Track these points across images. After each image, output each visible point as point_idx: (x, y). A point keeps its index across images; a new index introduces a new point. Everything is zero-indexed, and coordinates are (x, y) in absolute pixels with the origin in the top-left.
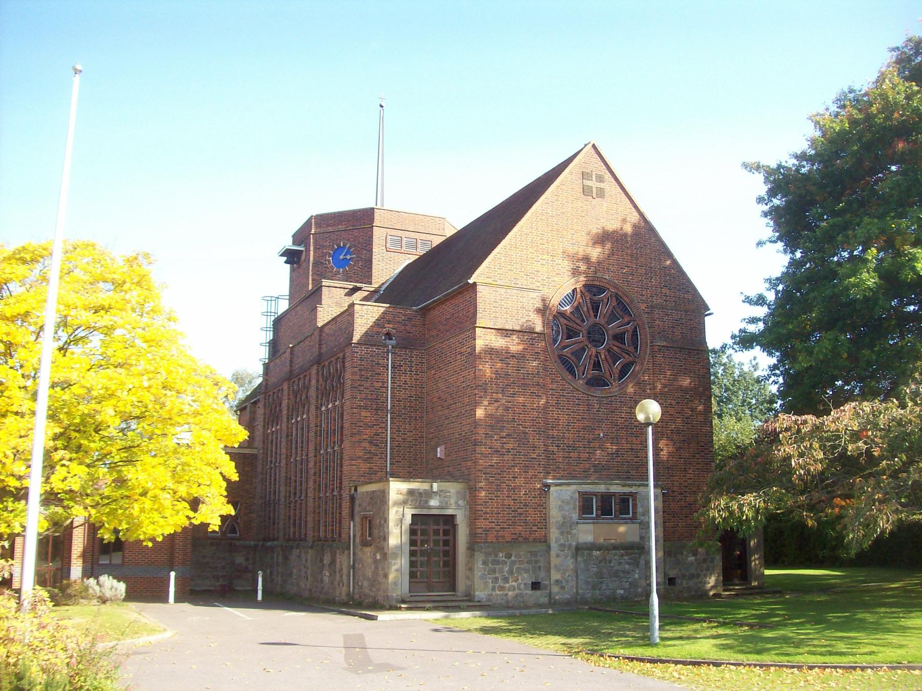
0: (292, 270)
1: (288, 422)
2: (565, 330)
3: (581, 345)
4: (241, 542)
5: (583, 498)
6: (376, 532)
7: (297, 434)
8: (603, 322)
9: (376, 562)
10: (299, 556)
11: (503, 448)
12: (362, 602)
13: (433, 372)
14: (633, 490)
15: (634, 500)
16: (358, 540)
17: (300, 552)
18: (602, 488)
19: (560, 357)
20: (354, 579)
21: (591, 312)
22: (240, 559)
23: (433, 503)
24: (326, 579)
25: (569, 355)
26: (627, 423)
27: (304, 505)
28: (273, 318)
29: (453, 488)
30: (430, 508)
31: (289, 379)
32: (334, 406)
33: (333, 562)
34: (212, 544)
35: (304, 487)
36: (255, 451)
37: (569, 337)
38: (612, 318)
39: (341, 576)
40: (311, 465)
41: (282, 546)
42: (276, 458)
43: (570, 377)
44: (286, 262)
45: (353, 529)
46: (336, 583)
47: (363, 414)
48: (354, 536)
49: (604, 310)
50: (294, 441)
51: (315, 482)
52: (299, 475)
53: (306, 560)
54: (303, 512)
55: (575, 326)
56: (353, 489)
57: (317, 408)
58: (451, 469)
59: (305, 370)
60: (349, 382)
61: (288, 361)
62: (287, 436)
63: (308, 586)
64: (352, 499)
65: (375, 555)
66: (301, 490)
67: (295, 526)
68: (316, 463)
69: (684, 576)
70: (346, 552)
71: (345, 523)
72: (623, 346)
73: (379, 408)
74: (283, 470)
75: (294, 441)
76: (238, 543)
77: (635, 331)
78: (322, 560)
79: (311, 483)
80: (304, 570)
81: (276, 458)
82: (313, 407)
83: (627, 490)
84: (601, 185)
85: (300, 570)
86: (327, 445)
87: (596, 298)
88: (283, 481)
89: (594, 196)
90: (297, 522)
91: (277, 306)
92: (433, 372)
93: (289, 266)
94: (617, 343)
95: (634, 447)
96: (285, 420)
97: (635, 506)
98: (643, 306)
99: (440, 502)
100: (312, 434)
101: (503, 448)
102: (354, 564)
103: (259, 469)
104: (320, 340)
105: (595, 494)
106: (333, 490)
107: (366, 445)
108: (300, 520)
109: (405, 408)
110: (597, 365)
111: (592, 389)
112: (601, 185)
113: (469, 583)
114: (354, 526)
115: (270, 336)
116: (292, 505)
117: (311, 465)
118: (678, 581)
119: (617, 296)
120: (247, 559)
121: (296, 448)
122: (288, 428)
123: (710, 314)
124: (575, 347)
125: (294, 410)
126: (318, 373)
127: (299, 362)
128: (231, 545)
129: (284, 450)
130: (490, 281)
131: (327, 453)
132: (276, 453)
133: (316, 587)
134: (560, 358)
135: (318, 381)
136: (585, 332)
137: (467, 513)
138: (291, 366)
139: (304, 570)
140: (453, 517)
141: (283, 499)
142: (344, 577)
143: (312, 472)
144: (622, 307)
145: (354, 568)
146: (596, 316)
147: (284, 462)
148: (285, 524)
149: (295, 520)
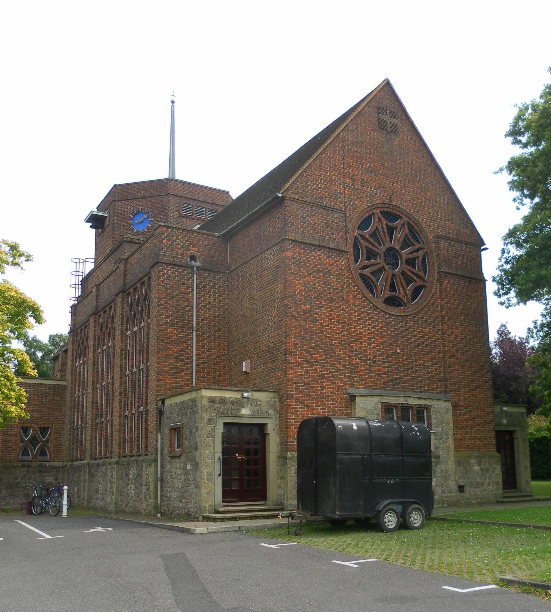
0: (97, 235)
1: (94, 352)
2: (365, 251)
3: (378, 267)
4: (51, 463)
5: (385, 409)
6: (186, 442)
7: (103, 362)
8: (397, 247)
9: (186, 473)
10: (105, 473)
11: (311, 358)
12: (168, 514)
13: (237, 292)
14: (427, 402)
15: (429, 412)
16: (166, 452)
17: (106, 469)
18: (401, 401)
19: (361, 275)
20: (161, 491)
21: (387, 235)
22: (49, 479)
23: (245, 411)
24: (132, 492)
25: (369, 275)
26: (419, 341)
27: (109, 425)
28: (81, 278)
29: (262, 396)
30: (241, 417)
31: (95, 314)
32: (140, 329)
33: (139, 476)
34: (23, 466)
35: (109, 409)
36: (64, 383)
37: (368, 258)
38: (406, 244)
39: (148, 489)
40: (117, 386)
41: (89, 464)
42: (83, 387)
43: (370, 295)
44: (91, 227)
45: (159, 441)
46: (143, 496)
47: (170, 330)
48: (162, 448)
49: (399, 235)
50: (100, 368)
51: (121, 402)
52: (104, 398)
53: (112, 476)
54: (109, 431)
55: (373, 248)
56: (160, 403)
57: (122, 333)
58: (257, 381)
59: (110, 304)
60: (156, 300)
61: (95, 299)
62: (94, 364)
63: (114, 501)
64: (161, 413)
65: (185, 466)
66: (107, 411)
67: (101, 445)
68: (121, 384)
69: (471, 484)
70: (153, 465)
71: (151, 438)
72: (413, 270)
73: (186, 326)
74: (90, 396)
75: (100, 368)
76: (47, 464)
77: (424, 258)
78: (127, 475)
79: (116, 403)
80: (109, 485)
81: (83, 387)
82: (118, 333)
83: (422, 402)
84: (395, 121)
85: (106, 485)
86: (132, 366)
87: (391, 224)
88: (89, 405)
89: (389, 130)
90: (103, 441)
91: (84, 267)
92: (237, 292)
93: (94, 230)
94: (409, 268)
95: (426, 363)
96: (91, 350)
97: (429, 418)
98: (430, 236)
99: (252, 411)
100: (117, 357)
101: (311, 358)
102: (162, 476)
103: (68, 398)
104: (125, 271)
105: (396, 406)
106: (139, 407)
107: (172, 360)
108: (106, 439)
109: (209, 327)
110: (393, 287)
111: (390, 308)
112: (395, 121)
113: (280, 492)
114: (162, 439)
115: (79, 293)
116: (99, 426)
117: (117, 386)
118: (467, 489)
119: (410, 226)
120: (56, 479)
121: (102, 374)
122: (94, 357)
123: (486, 249)
124: (374, 268)
125: (99, 341)
126: (123, 301)
127: (105, 297)
128: (41, 466)
129: (90, 378)
130: (297, 197)
131: (132, 373)
132: (83, 382)
133: (122, 501)
134: (361, 277)
135: (123, 308)
136: (382, 255)
137: (278, 422)
138: (97, 302)
139: (109, 485)
140: (262, 427)
141: (89, 422)
142: (152, 489)
143: (117, 392)
144: (414, 234)
145: (162, 480)
146: (391, 242)
147: (90, 388)
148: (91, 444)
149: (101, 440)
